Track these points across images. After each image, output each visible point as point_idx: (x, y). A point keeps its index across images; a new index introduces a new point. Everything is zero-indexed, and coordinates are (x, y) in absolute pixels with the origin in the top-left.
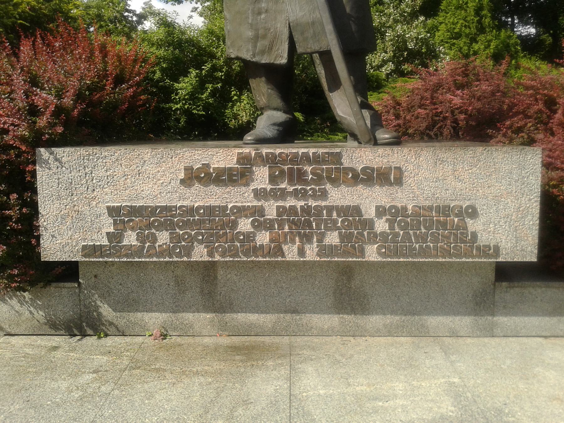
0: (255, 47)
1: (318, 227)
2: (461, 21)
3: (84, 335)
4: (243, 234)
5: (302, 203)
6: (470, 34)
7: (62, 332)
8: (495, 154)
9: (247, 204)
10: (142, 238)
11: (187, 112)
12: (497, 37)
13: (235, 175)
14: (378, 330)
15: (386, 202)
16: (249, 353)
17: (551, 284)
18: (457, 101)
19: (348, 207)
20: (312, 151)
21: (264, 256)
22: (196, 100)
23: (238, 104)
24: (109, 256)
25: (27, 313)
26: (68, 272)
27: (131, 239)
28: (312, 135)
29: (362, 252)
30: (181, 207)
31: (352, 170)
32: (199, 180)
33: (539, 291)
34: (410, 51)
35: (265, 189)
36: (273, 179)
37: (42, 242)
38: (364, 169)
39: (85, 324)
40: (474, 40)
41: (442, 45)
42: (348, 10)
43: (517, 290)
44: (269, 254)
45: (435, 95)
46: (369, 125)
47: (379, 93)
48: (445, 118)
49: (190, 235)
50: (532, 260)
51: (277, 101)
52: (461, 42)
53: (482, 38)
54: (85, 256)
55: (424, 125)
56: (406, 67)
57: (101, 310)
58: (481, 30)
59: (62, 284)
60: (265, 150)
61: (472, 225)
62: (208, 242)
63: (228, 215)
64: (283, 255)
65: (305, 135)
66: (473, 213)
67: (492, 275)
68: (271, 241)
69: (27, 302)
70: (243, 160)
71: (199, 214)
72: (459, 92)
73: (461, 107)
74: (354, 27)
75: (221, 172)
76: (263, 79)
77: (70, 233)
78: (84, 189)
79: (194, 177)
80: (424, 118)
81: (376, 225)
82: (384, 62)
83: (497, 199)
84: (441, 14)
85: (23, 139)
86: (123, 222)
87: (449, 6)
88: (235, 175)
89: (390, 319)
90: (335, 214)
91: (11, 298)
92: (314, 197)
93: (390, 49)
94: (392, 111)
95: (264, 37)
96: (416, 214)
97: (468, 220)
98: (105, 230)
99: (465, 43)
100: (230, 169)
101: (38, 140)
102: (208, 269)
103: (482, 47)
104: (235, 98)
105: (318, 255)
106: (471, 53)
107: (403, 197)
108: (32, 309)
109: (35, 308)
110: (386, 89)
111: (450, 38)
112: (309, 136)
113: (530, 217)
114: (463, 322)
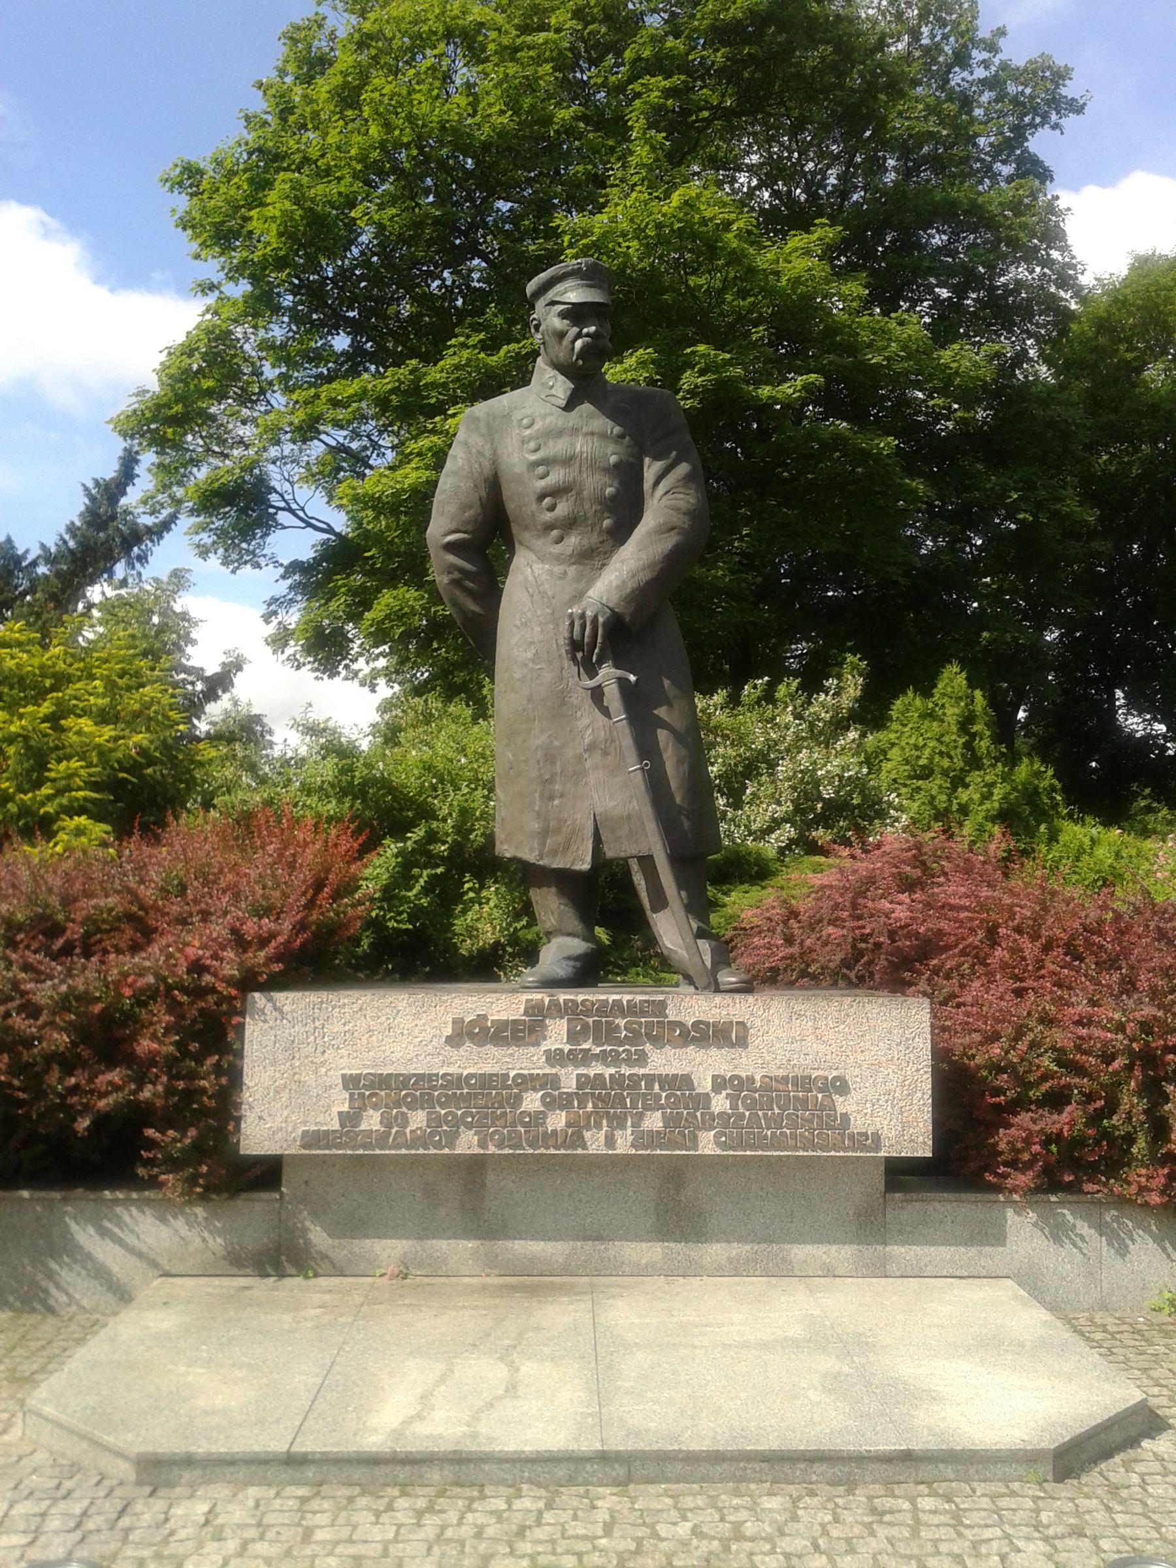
0: (544, 844)
1: (634, 1105)
2: (932, 744)
3: (283, 1275)
4: (529, 1115)
5: (612, 1071)
6: (949, 769)
7: (249, 1271)
8: (868, 1007)
9: (536, 1072)
10: (387, 1122)
11: (375, 925)
12: (1005, 778)
13: (521, 1031)
14: (720, 1267)
15: (726, 1070)
16: (533, 1283)
17: (964, 1196)
18: (901, 914)
19: (675, 1076)
20: (626, 998)
21: (556, 1148)
22: (396, 902)
23: (477, 907)
24: (338, 1146)
25: (198, 1240)
26: (266, 1174)
27: (372, 1121)
28: (624, 971)
29: (695, 1139)
30: (445, 1075)
31: (680, 1024)
32: (472, 1036)
33: (949, 1206)
34: (828, 803)
35: (561, 1050)
36: (573, 1037)
37: (243, 1125)
38: (696, 1024)
39: (281, 1258)
40: (958, 782)
41: (896, 789)
42: (678, 800)
43: (917, 1205)
44: (564, 1145)
45: (860, 901)
46: (709, 964)
47: (763, 888)
48: (878, 945)
49: (455, 1116)
50: (920, 1154)
51: (575, 924)
52: (934, 786)
53: (975, 777)
54: (304, 1147)
55: (838, 957)
56: (820, 835)
57: (311, 1236)
58: (974, 762)
59: (256, 1195)
60: (563, 996)
61: (843, 1105)
62: (479, 1126)
63: (509, 1087)
64: (584, 1147)
65: (610, 972)
66: (841, 1086)
67: (878, 1180)
68: (569, 1125)
69: (199, 1224)
70: (534, 1009)
71: (469, 1085)
72: (904, 897)
73: (907, 926)
74: (686, 824)
75: (502, 1025)
76: (553, 890)
77: (285, 1113)
78: (310, 1049)
79: (468, 1033)
80: (839, 945)
81: (713, 1102)
82: (775, 824)
83: (875, 1066)
84: (895, 726)
85: (229, 981)
86: (362, 1096)
87: (908, 710)
88: (521, 1031)
89: (737, 1249)
90: (657, 1086)
91: (175, 1217)
92: (629, 1062)
93: (787, 796)
94: (779, 929)
95: (558, 831)
96: (766, 1088)
97: (836, 1097)
98: (335, 1110)
99: (940, 787)
100: (514, 1021)
101: (249, 982)
102: (476, 1166)
103: (976, 797)
104: (471, 895)
105: (633, 1146)
106: (955, 807)
107: (746, 1064)
108: (206, 1234)
109: (211, 1232)
110: (779, 880)
111: (910, 777)
112: (618, 974)
113: (919, 1094)
114: (842, 1254)
